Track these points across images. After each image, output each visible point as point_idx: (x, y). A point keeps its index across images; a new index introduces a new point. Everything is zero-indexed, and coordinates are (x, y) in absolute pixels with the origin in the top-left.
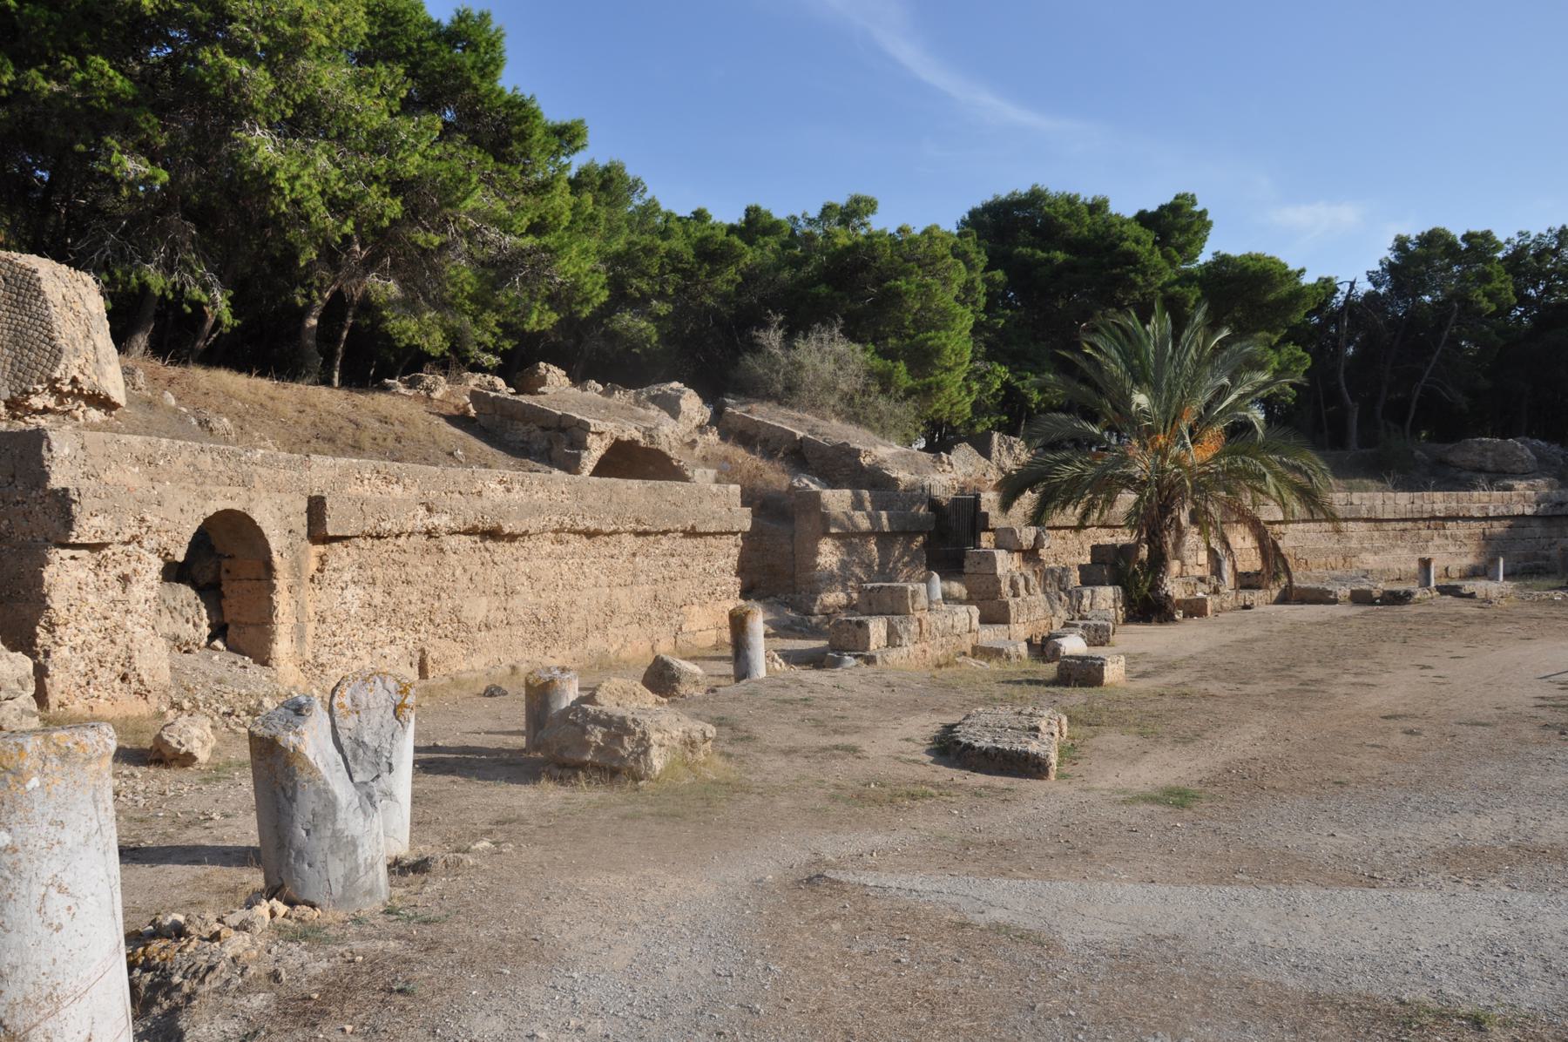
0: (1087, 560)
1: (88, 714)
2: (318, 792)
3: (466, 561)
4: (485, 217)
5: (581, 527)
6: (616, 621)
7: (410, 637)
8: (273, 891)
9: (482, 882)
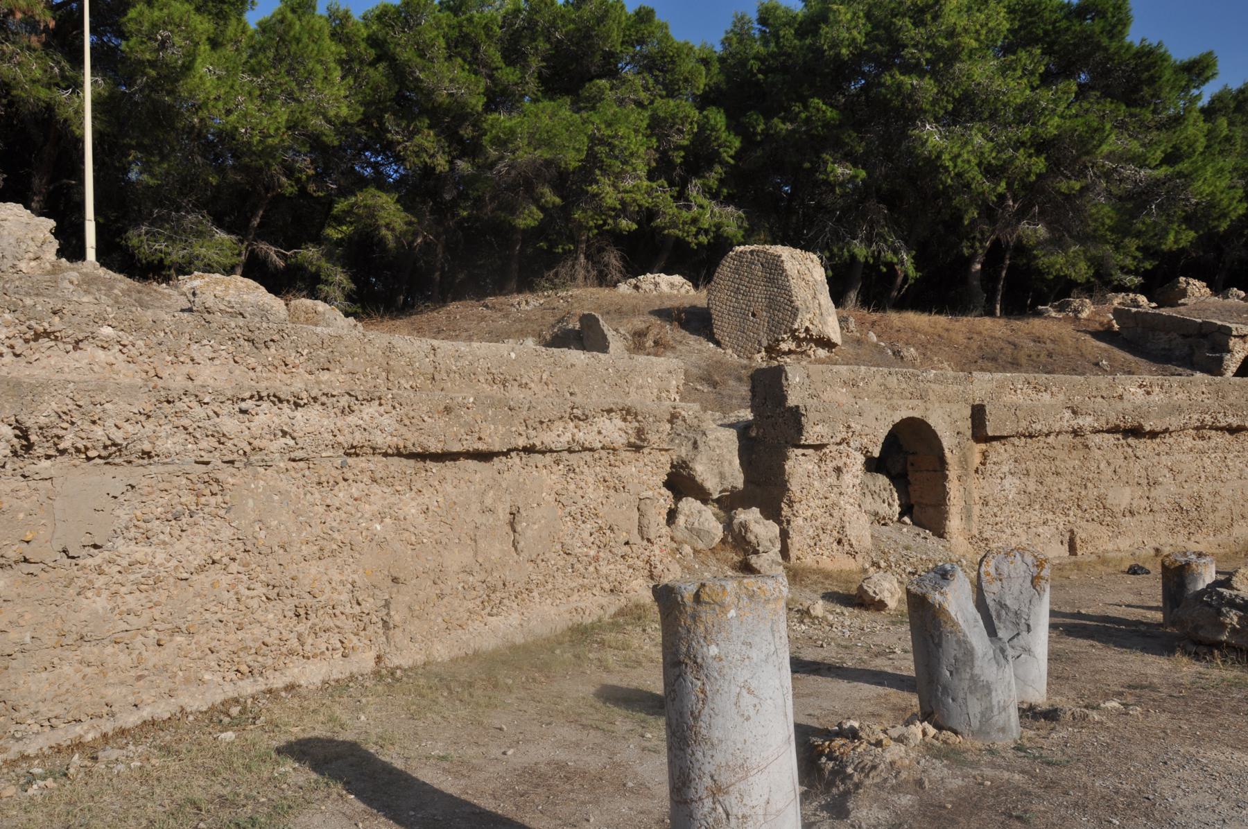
1: (815, 566)
2: (958, 642)
3: (1109, 456)
4: (1121, 158)
5: (1223, 424)
7: (1061, 520)
8: (927, 716)
9: (1104, 737)
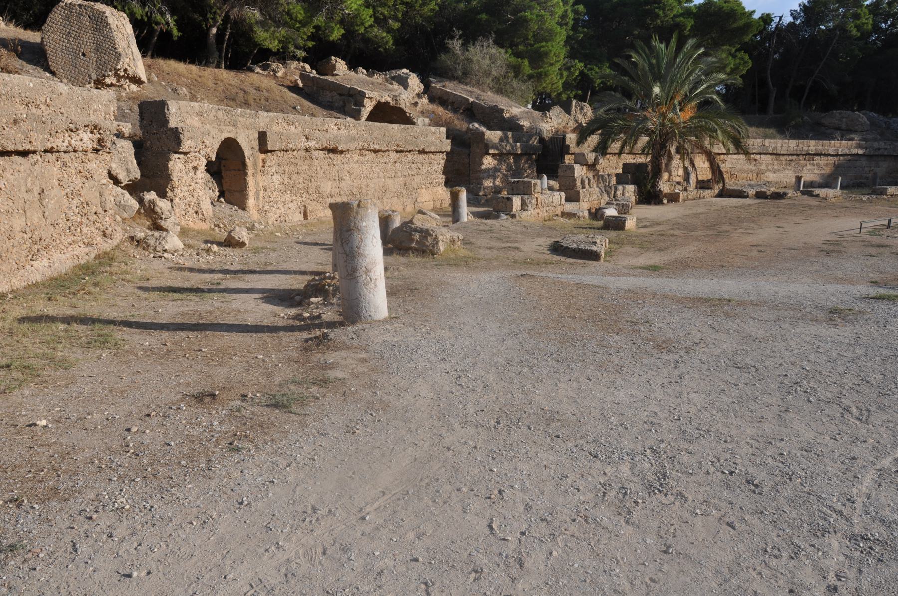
0: (620, 171)
6: (387, 196)
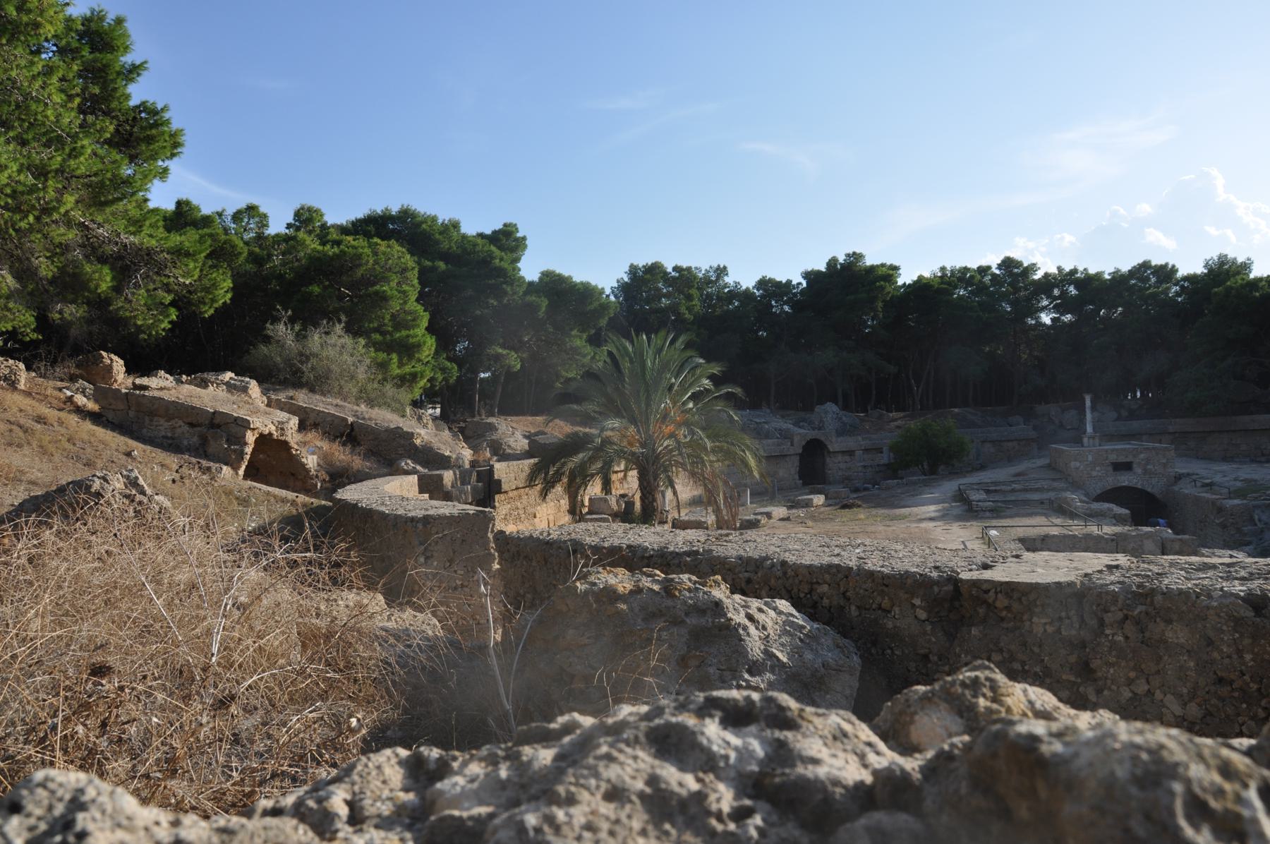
0: (427, 496)
